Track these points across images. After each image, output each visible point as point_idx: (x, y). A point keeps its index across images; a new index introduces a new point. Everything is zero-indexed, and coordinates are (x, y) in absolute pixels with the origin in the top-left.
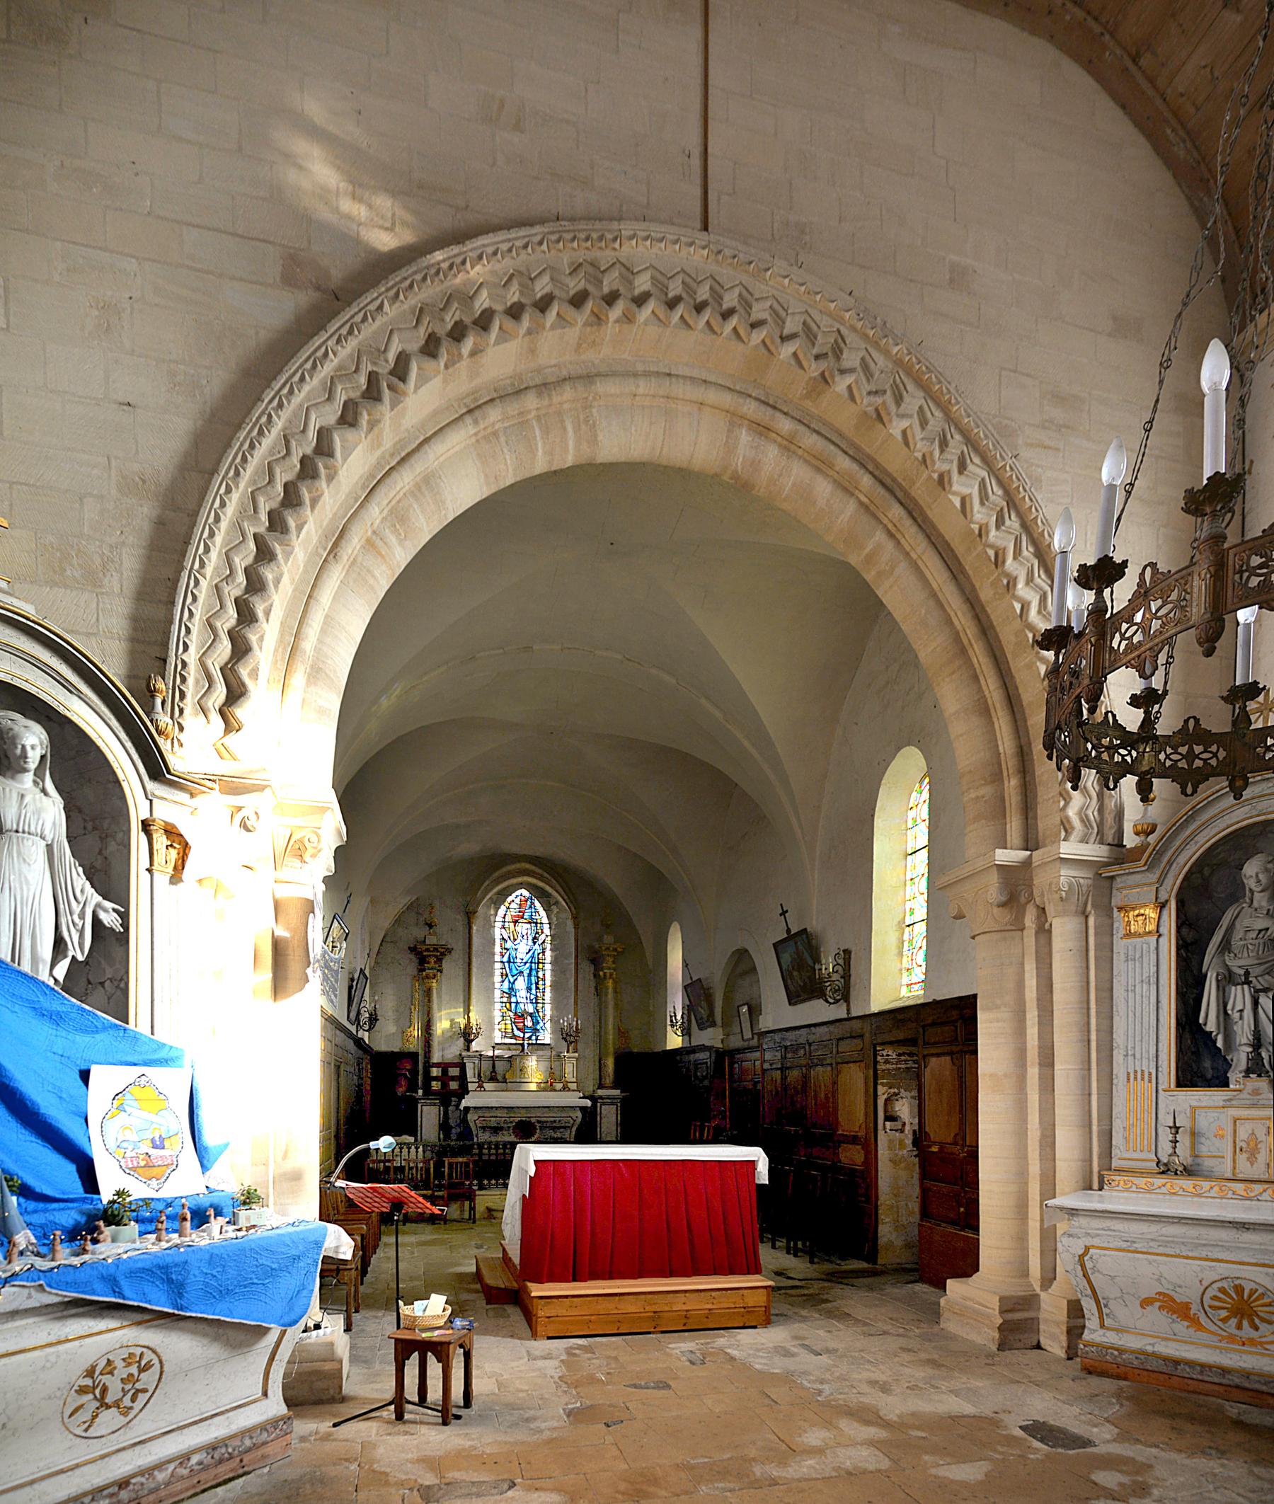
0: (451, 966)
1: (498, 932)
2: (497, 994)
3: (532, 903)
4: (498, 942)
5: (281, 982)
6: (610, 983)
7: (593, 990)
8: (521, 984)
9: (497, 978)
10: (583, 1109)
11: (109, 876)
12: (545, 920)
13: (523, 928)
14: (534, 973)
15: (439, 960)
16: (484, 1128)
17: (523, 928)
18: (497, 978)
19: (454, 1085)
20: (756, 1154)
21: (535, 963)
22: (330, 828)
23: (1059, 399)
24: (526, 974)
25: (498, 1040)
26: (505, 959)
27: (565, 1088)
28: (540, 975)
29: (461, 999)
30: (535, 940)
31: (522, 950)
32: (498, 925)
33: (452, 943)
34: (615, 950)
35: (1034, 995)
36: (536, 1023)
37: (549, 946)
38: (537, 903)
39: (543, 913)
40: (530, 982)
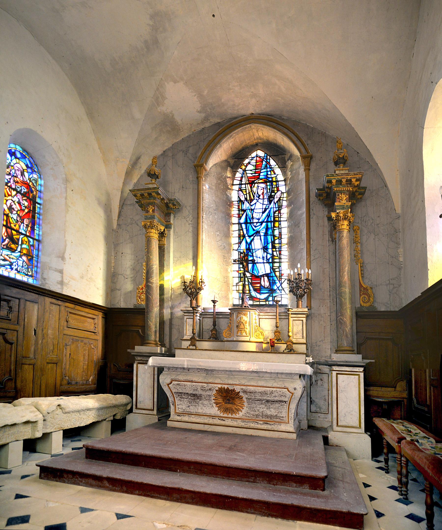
0: (180, 225)
3: (268, 163)
6: (344, 225)
7: (327, 237)
8: (257, 244)
9: (234, 240)
12: (281, 178)
13: (260, 188)
14: (270, 232)
15: (167, 215)
16: (180, 394)
17: (260, 188)
24: (262, 234)
26: (243, 220)
27: (290, 350)
28: (276, 233)
29: (191, 256)
30: (271, 199)
33: (178, 196)
34: (349, 182)
35: (364, 412)
36: (272, 283)
37: (285, 203)
38: (272, 163)
39: (278, 171)
40: (266, 242)
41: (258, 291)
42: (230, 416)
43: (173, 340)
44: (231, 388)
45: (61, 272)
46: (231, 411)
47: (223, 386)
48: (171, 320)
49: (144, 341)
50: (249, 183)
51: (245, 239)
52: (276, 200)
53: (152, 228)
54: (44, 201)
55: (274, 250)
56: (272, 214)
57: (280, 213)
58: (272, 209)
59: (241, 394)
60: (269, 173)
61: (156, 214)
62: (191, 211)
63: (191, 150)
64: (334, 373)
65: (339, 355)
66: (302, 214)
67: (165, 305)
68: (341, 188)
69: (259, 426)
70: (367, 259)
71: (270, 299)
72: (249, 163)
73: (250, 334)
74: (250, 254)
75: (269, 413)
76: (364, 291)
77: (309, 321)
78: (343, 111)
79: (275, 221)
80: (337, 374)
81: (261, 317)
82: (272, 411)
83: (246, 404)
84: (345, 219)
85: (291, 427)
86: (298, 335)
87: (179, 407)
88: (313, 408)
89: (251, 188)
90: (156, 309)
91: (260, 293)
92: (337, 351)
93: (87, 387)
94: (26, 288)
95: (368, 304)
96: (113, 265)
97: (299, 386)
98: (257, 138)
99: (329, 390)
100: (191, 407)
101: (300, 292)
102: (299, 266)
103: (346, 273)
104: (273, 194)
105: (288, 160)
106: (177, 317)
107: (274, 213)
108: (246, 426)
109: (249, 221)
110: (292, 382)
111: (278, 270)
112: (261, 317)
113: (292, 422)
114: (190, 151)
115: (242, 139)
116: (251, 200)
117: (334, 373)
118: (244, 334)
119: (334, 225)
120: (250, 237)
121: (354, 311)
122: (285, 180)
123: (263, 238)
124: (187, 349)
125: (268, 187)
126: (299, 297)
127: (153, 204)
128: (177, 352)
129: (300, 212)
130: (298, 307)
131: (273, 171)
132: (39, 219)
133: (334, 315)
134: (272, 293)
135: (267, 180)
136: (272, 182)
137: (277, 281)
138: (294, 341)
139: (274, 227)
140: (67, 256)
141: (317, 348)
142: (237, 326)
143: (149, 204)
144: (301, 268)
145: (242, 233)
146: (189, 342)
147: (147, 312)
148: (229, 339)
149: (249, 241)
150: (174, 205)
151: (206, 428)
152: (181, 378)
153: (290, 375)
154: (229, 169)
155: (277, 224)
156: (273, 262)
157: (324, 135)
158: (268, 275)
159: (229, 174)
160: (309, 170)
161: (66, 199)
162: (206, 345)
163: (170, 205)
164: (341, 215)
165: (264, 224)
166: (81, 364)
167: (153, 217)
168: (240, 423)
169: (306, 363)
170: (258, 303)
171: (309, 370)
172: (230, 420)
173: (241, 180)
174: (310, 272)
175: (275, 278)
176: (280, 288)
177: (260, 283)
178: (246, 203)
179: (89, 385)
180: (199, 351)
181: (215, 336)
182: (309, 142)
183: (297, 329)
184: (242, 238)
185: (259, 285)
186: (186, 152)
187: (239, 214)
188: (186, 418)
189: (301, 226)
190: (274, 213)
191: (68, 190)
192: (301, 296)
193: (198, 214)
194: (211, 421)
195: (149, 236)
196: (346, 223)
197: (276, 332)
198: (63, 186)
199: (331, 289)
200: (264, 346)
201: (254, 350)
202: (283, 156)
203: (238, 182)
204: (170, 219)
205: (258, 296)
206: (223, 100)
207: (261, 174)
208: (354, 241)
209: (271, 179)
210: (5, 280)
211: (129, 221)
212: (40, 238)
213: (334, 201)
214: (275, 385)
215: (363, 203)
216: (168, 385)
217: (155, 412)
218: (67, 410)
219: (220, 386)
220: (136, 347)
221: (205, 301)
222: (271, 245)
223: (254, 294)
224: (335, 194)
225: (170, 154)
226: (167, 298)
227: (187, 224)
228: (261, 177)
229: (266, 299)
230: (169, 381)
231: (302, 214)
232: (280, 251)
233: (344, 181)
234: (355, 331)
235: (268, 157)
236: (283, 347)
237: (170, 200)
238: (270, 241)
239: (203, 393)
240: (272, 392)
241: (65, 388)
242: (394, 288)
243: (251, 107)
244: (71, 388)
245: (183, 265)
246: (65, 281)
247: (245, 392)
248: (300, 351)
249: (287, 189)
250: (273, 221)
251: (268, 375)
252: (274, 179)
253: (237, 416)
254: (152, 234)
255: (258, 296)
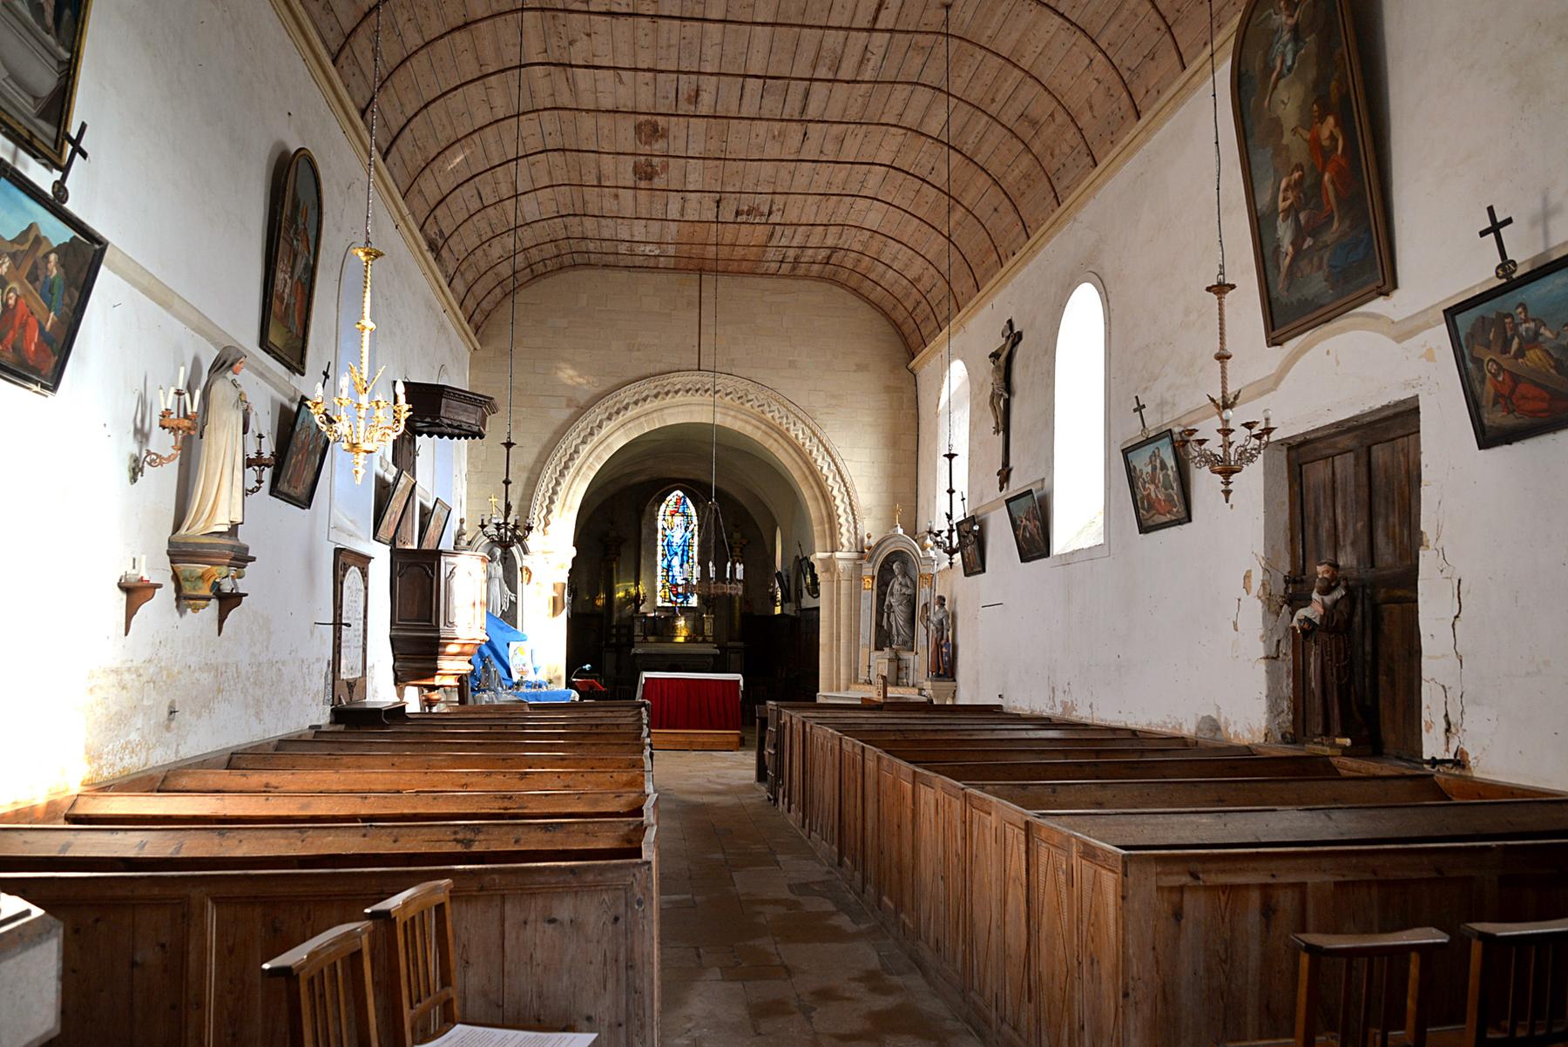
1: (660, 524)
2: (659, 569)
5: (555, 613)
8: (676, 561)
10: (714, 656)
11: (513, 588)
13: (678, 519)
17: (678, 519)
18: (659, 557)
19: (624, 640)
20: (739, 677)
21: (686, 546)
22: (573, 552)
23: (833, 396)
25: (659, 604)
27: (704, 641)
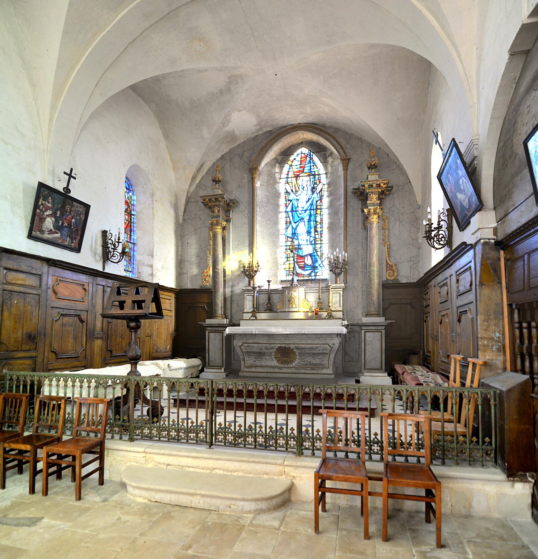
0: (238, 217)
3: (311, 159)
4: (283, 195)
6: (374, 219)
7: (361, 225)
8: (302, 229)
9: (282, 225)
12: (322, 171)
13: (304, 181)
14: (313, 218)
15: (227, 211)
16: (249, 353)
17: (304, 181)
18: (282, 225)
24: (306, 220)
27: (330, 317)
28: (318, 219)
30: (313, 189)
31: (303, 200)
32: (283, 181)
34: (379, 186)
36: (314, 261)
37: (325, 194)
38: (315, 158)
41: (302, 268)
42: (286, 366)
43: (233, 313)
44: (287, 346)
45: (151, 266)
46: (288, 363)
47: (282, 345)
48: (231, 296)
49: (211, 314)
50: (295, 177)
51: (291, 226)
52: (318, 190)
53: (218, 225)
54: (137, 212)
55: (316, 233)
56: (314, 203)
57: (321, 202)
58: (315, 199)
59: (294, 350)
60: (312, 167)
61: (221, 214)
62: (247, 206)
63: (246, 154)
64: (363, 332)
65: (367, 318)
66: (340, 205)
67: (227, 285)
68: (372, 190)
69: (308, 372)
70: (393, 241)
71: (313, 274)
72: (295, 159)
73: (299, 305)
74: (295, 237)
75: (314, 362)
76: (389, 267)
77: (345, 293)
78: (375, 128)
79: (317, 209)
80: (365, 332)
81: (306, 291)
82: (317, 361)
83: (298, 357)
84: (375, 214)
85: (330, 371)
86: (336, 304)
87: (248, 362)
88: (347, 358)
89: (296, 180)
90: (221, 290)
91: (304, 270)
92: (367, 315)
93: (165, 354)
94: (60, 265)
95: (393, 278)
96: (180, 253)
97: (337, 342)
98: (302, 139)
99: (360, 344)
100: (257, 362)
101: (338, 271)
102: (337, 250)
103: (374, 256)
104: (315, 186)
105: (329, 156)
106: (236, 294)
107: (317, 202)
108: (298, 372)
109: (294, 210)
110: (332, 340)
111: (319, 250)
112: (306, 291)
113: (331, 367)
114: (245, 155)
115: (290, 141)
116: (297, 191)
117: (363, 332)
118: (294, 306)
119: (366, 218)
120: (295, 223)
121: (381, 283)
122: (326, 174)
123: (306, 223)
124: (249, 320)
125: (312, 180)
126: (337, 275)
127: (218, 206)
128: (242, 322)
129: (338, 203)
130: (336, 283)
131: (316, 165)
132: (133, 226)
133: (365, 287)
134: (314, 270)
135: (312, 174)
136: (315, 175)
137: (319, 260)
138: (333, 309)
139: (316, 214)
140: (154, 254)
141: (351, 313)
142: (289, 301)
143: (214, 206)
144: (339, 253)
145: (288, 220)
146: (251, 314)
147: (215, 293)
148: (282, 310)
149: (294, 227)
150: (234, 203)
151: (269, 375)
152: (250, 341)
153: (330, 335)
154: (277, 165)
155: (319, 211)
156: (315, 244)
157: (360, 140)
158: (311, 255)
159: (277, 170)
160: (347, 169)
161: (153, 209)
162: (262, 316)
163: (231, 204)
164: (372, 211)
165: (308, 212)
166: (163, 336)
167: (218, 216)
168: (294, 370)
169: (343, 326)
170: (302, 278)
171: (344, 331)
172: (286, 369)
173: (288, 174)
174: (346, 255)
175: (317, 257)
176: (321, 265)
177: (304, 262)
178: (292, 193)
179: (167, 352)
180: (259, 321)
181: (270, 308)
182: (348, 146)
183: (335, 300)
184: (288, 224)
185: (303, 263)
186: (241, 156)
187: (286, 204)
188: (253, 370)
189: (339, 215)
190: (317, 202)
191: (154, 201)
192: (339, 274)
193: (253, 209)
194: (272, 370)
195: (216, 232)
196: (376, 216)
197: (318, 303)
198: (150, 199)
199: (363, 267)
200: (310, 314)
201: (303, 318)
202: (325, 152)
203: (286, 176)
204: (229, 214)
205: (302, 272)
206: (276, 117)
207: (305, 169)
208: (383, 228)
209: (313, 173)
210: (89, 271)
211: (193, 216)
212: (135, 242)
213: (367, 199)
214: (319, 342)
215: (391, 196)
216: (240, 347)
217: (223, 370)
218: (172, 368)
219: (279, 345)
220: (207, 320)
221: (260, 281)
222: (314, 229)
223: (299, 271)
224: (367, 194)
225: (228, 158)
226: (228, 279)
227: (244, 217)
228: (305, 171)
229: (310, 275)
230: (240, 344)
231: (340, 205)
232: (321, 234)
233: (374, 185)
234: (381, 299)
235: (312, 153)
236: (325, 314)
237: (231, 200)
238: (312, 226)
239: (267, 351)
240: (317, 347)
241: (155, 355)
242: (414, 264)
243: (300, 119)
244: (158, 355)
245: (240, 252)
246: (154, 273)
247: (297, 348)
248: (338, 317)
249: (328, 181)
250: (315, 209)
251: (314, 336)
252: (317, 173)
253: (292, 366)
254: (218, 230)
255: (302, 272)
